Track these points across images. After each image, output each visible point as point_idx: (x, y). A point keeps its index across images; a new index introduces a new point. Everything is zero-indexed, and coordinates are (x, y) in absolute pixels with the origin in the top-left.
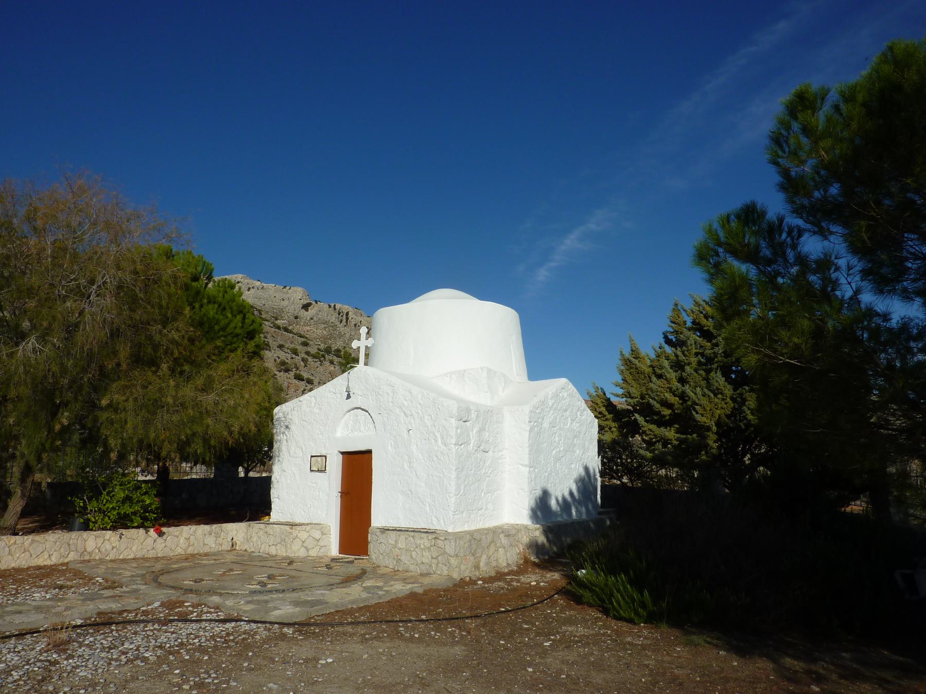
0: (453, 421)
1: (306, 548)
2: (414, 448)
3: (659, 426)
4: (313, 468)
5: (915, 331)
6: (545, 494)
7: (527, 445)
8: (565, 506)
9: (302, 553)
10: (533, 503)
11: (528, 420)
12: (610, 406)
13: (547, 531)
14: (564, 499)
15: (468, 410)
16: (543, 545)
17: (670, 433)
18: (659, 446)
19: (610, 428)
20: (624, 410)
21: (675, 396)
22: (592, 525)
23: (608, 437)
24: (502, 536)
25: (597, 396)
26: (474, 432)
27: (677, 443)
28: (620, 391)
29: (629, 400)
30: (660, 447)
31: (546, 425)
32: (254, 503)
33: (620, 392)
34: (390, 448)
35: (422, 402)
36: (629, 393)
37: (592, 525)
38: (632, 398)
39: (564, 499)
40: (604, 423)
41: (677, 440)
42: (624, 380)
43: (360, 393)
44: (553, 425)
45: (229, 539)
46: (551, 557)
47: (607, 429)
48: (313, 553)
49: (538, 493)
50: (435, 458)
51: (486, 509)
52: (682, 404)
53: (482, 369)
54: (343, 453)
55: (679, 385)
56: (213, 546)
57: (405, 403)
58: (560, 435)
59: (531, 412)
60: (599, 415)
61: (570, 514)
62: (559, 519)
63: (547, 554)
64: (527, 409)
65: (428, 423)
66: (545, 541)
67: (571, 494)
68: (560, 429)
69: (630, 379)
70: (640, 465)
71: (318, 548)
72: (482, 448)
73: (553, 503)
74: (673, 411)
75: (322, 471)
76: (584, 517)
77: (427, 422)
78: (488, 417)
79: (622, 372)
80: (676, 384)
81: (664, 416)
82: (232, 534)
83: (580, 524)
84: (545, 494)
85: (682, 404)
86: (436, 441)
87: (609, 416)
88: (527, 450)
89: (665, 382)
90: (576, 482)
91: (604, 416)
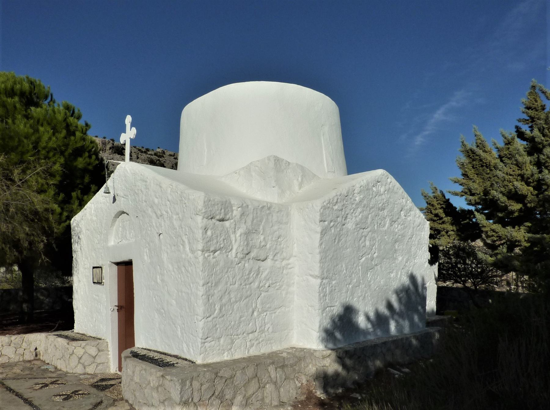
0: (199, 219)
1: (83, 364)
2: (165, 257)
3: (504, 225)
4: (96, 281)
5: (524, 267)
6: (349, 311)
7: (318, 251)
8: (380, 321)
9: (79, 370)
10: (327, 323)
11: (318, 218)
12: (449, 208)
13: (342, 357)
14: (378, 315)
15: (227, 206)
16: (337, 375)
17: (520, 234)
18: (504, 249)
19: (447, 232)
20: (463, 211)
21: (528, 184)
22: (414, 342)
23: (444, 243)
24: (271, 369)
25: (435, 197)
26: (238, 233)
27: (528, 245)
28: (459, 189)
29: (471, 198)
30: (505, 250)
31: (350, 225)
32: (58, 316)
33: (459, 189)
34: (146, 258)
35: (170, 198)
36: (470, 190)
37: (414, 342)
38: (472, 194)
39: (378, 315)
40: (439, 227)
41: (528, 241)
42: (465, 175)
43: (122, 194)
44: (361, 225)
45: (32, 349)
46: (348, 390)
47: (443, 233)
48: (90, 370)
49: (337, 309)
50: (183, 269)
51: (262, 331)
52: (537, 195)
53: (269, 158)
54: (118, 264)
55: (535, 169)
56: (12, 356)
57: (156, 201)
58: (372, 239)
59: (324, 208)
60: (433, 218)
61: (388, 330)
62: (371, 337)
63: (343, 385)
64: (318, 204)
65: (176, 224)
66: (340, 369)
67: (390, 306)
68: (373, 231)
69: (471, 173)
70: (483, 271)
71: (94, 365)
72: (252, 255)
73: (361, 321)
74: (525, 205)
75: (100, 283)
76: (407, 330)
77: (175, 223)
78: (260, 216)
79: (462, 165)
80: (530, 169)
81: (512, 212)
82: (36, 344)
83: (400, 343)
84: (349, 311)
85: (537, 195)
86: (183, 245)
87: (448, 219)
88: (318, 257)
89: (516, 168)
90: (397, 292)
91: (441, 218)
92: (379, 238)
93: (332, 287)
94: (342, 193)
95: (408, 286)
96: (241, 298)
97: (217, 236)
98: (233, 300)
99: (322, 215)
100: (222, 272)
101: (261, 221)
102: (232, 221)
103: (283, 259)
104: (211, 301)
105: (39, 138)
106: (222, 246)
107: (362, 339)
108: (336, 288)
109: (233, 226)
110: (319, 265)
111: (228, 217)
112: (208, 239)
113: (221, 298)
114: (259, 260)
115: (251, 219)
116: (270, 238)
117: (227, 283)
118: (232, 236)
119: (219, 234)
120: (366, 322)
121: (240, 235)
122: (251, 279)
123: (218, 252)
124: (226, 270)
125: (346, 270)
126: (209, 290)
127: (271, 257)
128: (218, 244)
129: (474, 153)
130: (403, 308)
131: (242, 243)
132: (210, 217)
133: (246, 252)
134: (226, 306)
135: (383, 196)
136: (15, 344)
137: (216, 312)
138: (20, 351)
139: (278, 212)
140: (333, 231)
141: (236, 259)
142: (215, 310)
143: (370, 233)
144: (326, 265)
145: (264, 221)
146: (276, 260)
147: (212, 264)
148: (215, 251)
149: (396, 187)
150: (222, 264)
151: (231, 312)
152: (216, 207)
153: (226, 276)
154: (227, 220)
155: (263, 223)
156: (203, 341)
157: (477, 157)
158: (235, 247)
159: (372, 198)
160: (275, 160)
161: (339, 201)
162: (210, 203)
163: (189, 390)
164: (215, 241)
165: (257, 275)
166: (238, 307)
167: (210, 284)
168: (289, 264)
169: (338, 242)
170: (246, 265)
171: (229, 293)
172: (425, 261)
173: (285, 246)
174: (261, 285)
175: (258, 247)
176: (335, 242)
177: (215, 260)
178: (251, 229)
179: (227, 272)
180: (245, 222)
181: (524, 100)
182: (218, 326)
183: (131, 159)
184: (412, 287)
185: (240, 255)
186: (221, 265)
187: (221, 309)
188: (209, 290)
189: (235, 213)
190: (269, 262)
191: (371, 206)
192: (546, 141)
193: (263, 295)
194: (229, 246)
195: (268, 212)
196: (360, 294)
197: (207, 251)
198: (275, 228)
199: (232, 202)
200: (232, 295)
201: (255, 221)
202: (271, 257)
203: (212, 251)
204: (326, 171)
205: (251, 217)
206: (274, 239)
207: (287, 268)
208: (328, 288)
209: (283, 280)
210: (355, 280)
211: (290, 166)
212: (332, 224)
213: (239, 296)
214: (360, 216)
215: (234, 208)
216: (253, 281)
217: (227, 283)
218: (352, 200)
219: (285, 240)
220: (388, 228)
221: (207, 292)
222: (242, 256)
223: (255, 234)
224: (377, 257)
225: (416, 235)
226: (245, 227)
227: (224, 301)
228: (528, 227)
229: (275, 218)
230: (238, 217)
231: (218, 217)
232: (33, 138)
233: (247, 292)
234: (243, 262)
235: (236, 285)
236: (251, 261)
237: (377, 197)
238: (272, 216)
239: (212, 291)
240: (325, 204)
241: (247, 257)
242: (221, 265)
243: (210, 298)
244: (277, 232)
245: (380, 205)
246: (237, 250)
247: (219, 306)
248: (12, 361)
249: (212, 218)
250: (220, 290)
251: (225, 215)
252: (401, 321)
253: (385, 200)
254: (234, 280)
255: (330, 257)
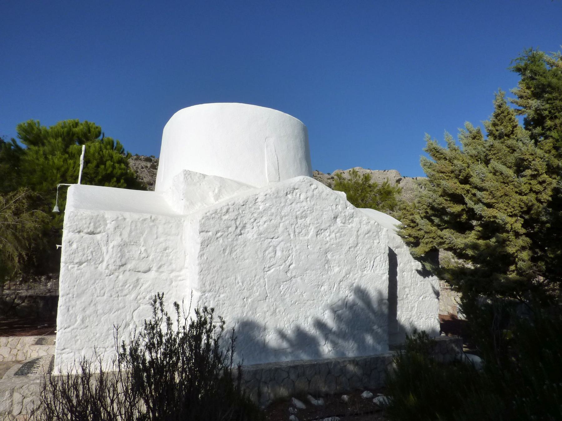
31: (250, 234)
56: (6, 356)
62: (286, 360)
72: (129, 266)
83: (328, 369)
92: (297, 247)
93: (219, 300)
94: (237, 202)
95: (354, 301)
96: (110, 310)
97: (84, 249)
98: (100, 311)
99: (202, 225)
100: (88, 283)
101: (142, 233)
102: (104, 234)
103: (172, 271)
104: (71, 312)
105: (68, 169)
106: (89, 258)
107: (272, 360)
108: (226, 302)
109: (105, 238)
110: (198, 277)
111: (98, 230)
112: (72, 252)
113: (84, 309)
114: (139, 272)
115: (128, 231)
116: (153, 249)
117: (93, 295)
118: (104, 249)
119: (86, 247)
120: (280, 341)
121: (113, 247)
122: (125, 292)
123: (85, 264)
124: (93, 281)
125: (243, 283)
126: (70, 301)
127: (154, 269)
128: (85, 256)
129: (438, 152)
130: (343, 326)
131: (114, 255)
132: (76, 231)
133: (118, 263)
134: (91, 318)
135: (304, 204)
136: (11, 345)
137: (77, 323)
138: (14, 352)
139: (165, 223)
140: (221, 241)
141: (107, 271)
142: (76, 321)
143: (282, 243)
144: (209, 277)
145: (146, 233)
146: (162, 272)
147: (75, 275)
148: (80, 263)
149: (324, 193)
150: (87, 275)
151: (96, 324)
152: (84, 221)
153: (93, 287)
154: (98, 233)
155: (144, 235)
156: (59, 351)
157: (442, 156)
158: (106, 258)
159: (284, 206)
160: (185, 174)
161: (231, 210)
162: (76, 218)
163: (8, 402)
164: (81, 253)
165: (135, 287)
166: (106, 320)
167: (70, 295)
168: (178, 276)
169: (231, 253)
170: (121, 277)
171: (95, 304)
172: (381, 272)
173: (174, 257)
174: (139, 297)
175: (137, 259)
176: (224, 253)
177: (79, 271)
178: (127, 241)
179: (94, 283)
180: (121, 235)
181: (515, 90)
182: (78, 337)
183: (81, 183)
184: (360, 303)
185: (112, 267)
186: (86, 276)
187: (83, 321)
188: (70, 301)
189: (109, 226)
190: (152, 274)
191: (283, 214)
192: (497, 130)
193: (141, 308)
194: (99, 258)
195: (151, 224)
196: (265, 309)
197: (71, 263)
198: (162, 239)
199: (106, 216)
200: (99, 307)
201: (133, 233)
202: (154, 269)
203: (77, 263)
204: (268, 181)
205: (128, 229)
206: (158, 250)
207: (176, 281)
208: (212, 302)
209: (170, 292)
210: (258, 294)
211: (206, 179)
212: (219, 234)
213: (108, 307)
214: (265, 226)
215: (108, 222)
216: (129, 293)
217: (93, 295)
218: (252, 209)
219: (174, 251)
220: (312, 237)
221: (66, 303)
222: (114, 268)
223: (134, 246)
224: (295, 268)
225: (363, 243)
226: (119, 239)
227: (88, 312)
228: (479, 231)
229: (160, 230)
230: (112, 230)
231: (85, 231)
232: (63, 169)
233: (118, 304)
234: (116, 274)
235: (105, 297)
236: (127, 273)
237: (293, 205)
238: (158, 228)
239: (73, 302)
240: (208, 214)
241: (122, 269)
242: (86, 276)
243: (70, 309)
244: (164, 244)
245: (298, 213)
246: (108, 262)
247: (81, 317)
248: (6, 360)
249: (79, 232)
250: (84, 302)
251: (95, 228)
252: (340, 342)
253: (306, 208)
254: (102, 292)
255: (215, 268)
